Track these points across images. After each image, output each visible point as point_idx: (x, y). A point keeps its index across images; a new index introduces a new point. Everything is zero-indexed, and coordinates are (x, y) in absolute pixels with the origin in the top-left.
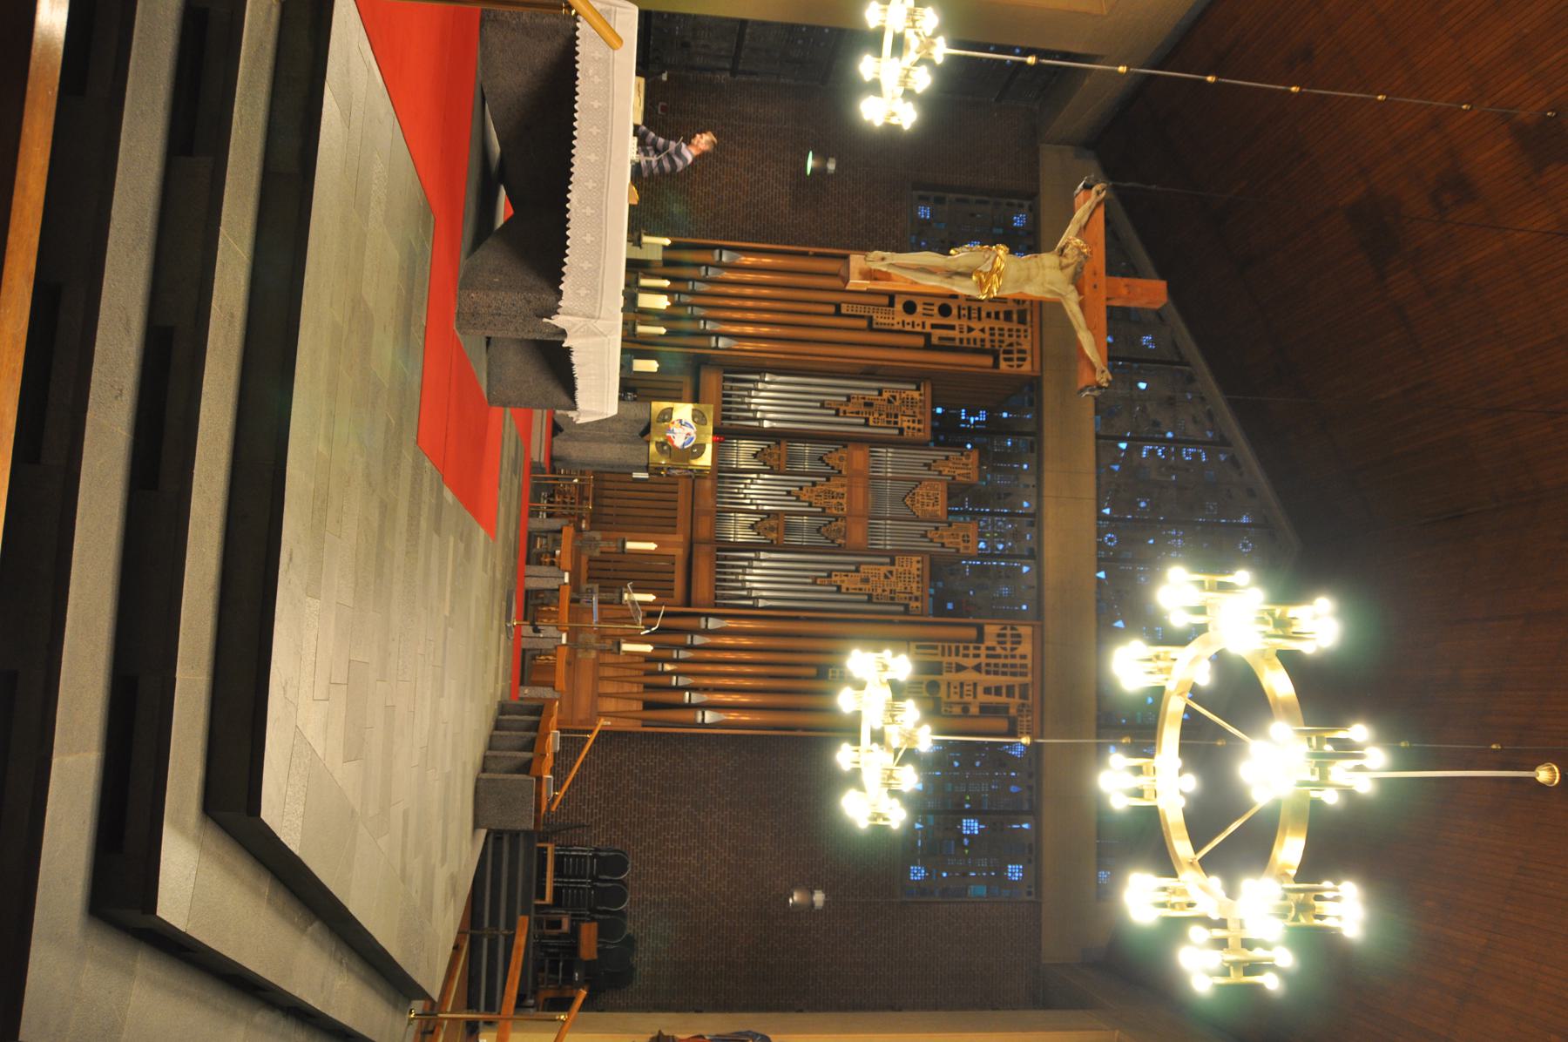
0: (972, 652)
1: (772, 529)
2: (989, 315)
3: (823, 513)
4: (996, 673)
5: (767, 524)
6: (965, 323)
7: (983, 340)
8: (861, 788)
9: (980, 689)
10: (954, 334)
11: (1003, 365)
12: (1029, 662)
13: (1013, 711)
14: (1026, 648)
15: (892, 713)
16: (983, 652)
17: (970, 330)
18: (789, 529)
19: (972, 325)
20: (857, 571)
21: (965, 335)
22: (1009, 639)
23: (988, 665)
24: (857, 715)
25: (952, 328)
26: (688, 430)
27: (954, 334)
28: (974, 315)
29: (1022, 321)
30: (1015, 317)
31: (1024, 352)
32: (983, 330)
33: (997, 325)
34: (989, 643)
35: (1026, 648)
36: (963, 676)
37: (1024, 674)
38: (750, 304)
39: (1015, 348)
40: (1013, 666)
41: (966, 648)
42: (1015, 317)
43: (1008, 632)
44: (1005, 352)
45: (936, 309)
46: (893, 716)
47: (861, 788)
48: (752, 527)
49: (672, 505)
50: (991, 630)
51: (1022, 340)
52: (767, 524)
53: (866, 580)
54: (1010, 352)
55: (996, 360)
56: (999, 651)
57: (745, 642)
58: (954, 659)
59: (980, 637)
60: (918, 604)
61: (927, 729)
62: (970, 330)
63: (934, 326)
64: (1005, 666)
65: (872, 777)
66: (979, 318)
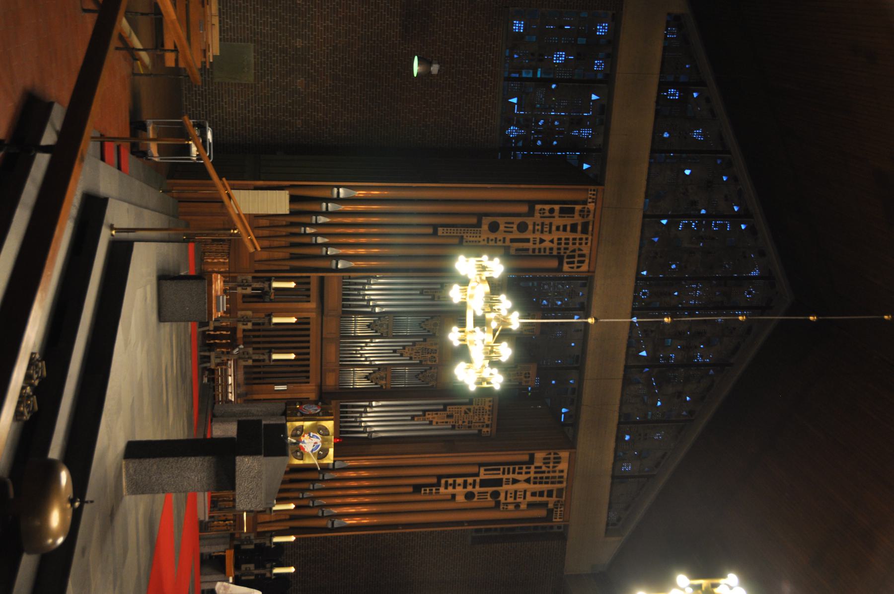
0: (524, 470)
1: (382, 378)
2: (558, 228)
3: (421, 364)
4: (541, 483)
5: (377, 375)
6: (538, 236)
7: (551, 249)
8: (469, 360)
9: (528, 494)
10: (530, 245)
11: (566, 267)
12: (565, 474)
13: (551, 506)
14: (564, 466)
15: (490, 302)
16: (533, 469)
17: (542, 241)
18: (395, 377)
19: (543, 237)
20: (445, 410)
21: (537, 246)
22: (552, 460)
23: (535, 478)
24: (464, 305)
25: (528, 240)
26: (315, 440)
27: (530, 245)
28: (546, 229)
29: (585, 230)
30: (579, 228)
31: (583, 256)
32: (552, 241)
33: (563, 235)
34: (537, 464)
35: (564, 466)
36: (516, 486)
37: (561, 482)
38: (362, 230)
39: (577, 253)
40: (553, 477)
41: (521, 468)
42: (579, 228)
43: (552, 456)
44: (569, 257)
45: (515, 226)
46: (491, 307)
47: (469, 360)
48: (367, 377)
49: (307, 357)
50: (540, 456)
51: (583, 247)
52: (377, 375)
53: (449, 416)
54: (573, 257)
55: (561, 263)
56: (544, 468)
57: (364, 474)
58: (511, 476)
59: (531, 460)
60: (489, 429)
61: (516, 314)
62: (542, 241)
63: (512, 241)
64: (547, 478)
65: (477, 353)
66: (550, 232)
